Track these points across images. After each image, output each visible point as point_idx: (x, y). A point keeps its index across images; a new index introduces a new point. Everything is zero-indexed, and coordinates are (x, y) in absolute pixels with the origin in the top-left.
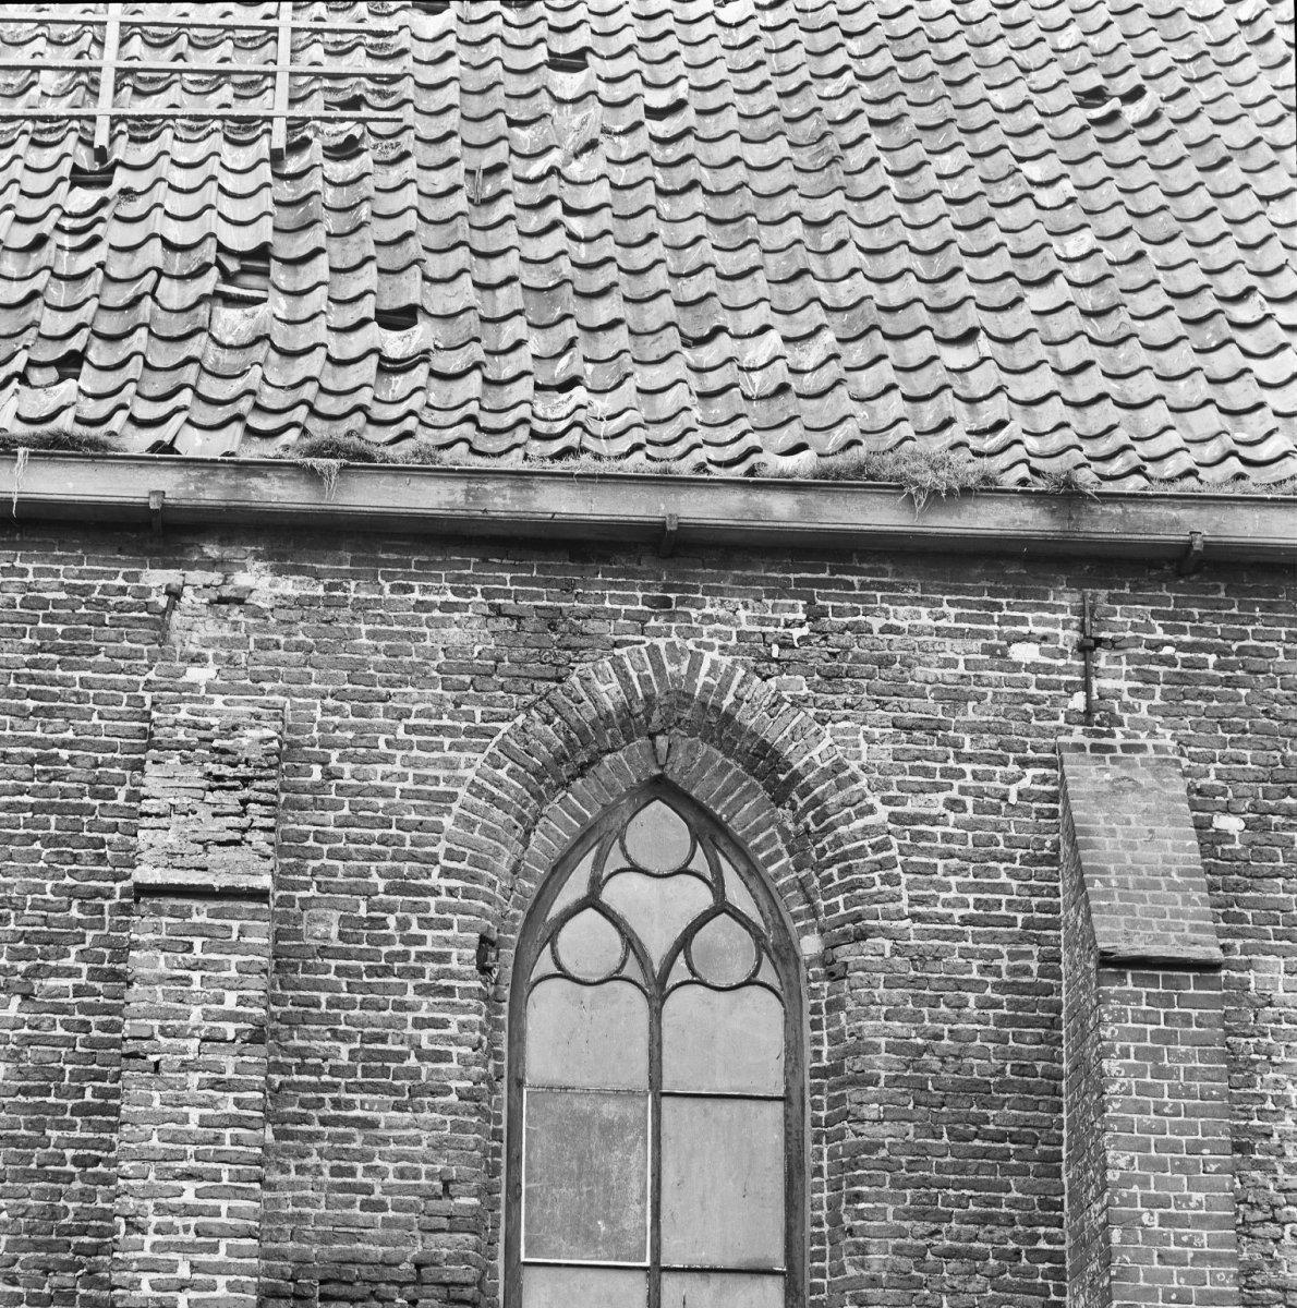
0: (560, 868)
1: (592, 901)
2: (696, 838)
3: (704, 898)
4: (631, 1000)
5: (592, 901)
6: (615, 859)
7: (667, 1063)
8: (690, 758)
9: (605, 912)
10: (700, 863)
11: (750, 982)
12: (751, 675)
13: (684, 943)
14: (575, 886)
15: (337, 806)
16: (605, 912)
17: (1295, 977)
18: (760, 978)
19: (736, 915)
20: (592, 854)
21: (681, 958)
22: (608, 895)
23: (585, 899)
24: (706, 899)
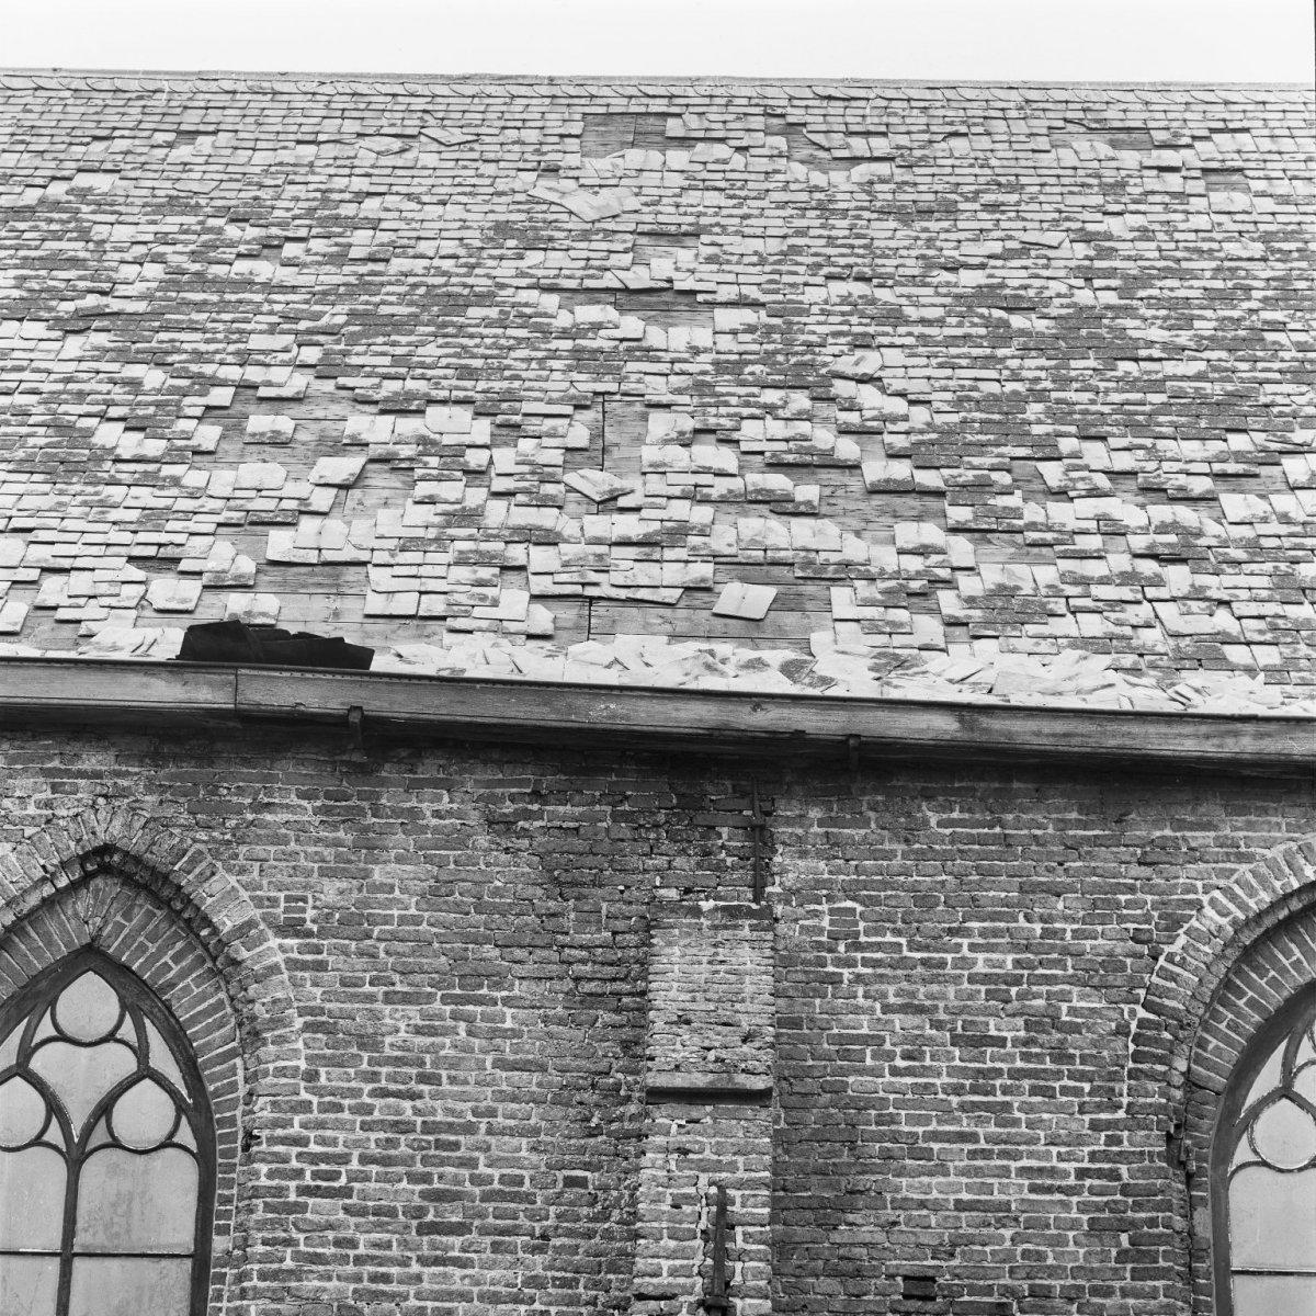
2: (124, 1007)
5: (1286, 1092)
6: (46, 1029)
10: (128, 1031)
13: (105, 1109)
19: (160, 1081)
21: (103, 1122)
22: (36, 1064)
24: (129, 1064)
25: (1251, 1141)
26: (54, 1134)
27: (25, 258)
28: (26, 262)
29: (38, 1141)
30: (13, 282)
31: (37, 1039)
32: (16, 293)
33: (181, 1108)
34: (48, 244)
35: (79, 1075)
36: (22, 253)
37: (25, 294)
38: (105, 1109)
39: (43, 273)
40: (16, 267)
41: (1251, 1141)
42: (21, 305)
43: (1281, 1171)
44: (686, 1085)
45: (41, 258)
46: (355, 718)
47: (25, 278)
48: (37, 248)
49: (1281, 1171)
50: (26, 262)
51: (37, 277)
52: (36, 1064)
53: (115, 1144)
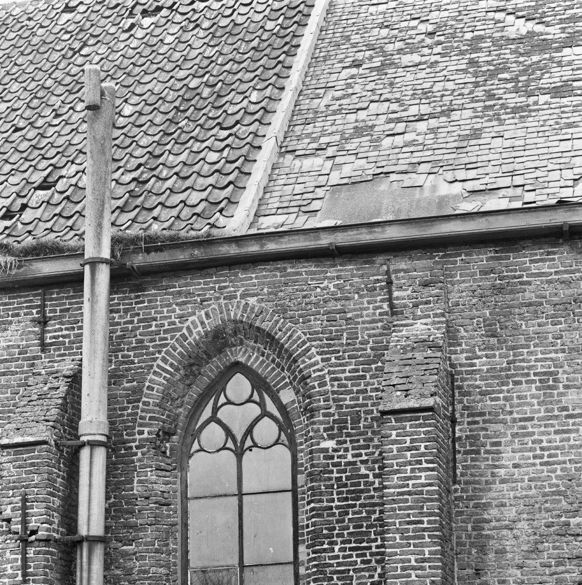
0: (199, 405)
1: (214, 418)
3: (256, 410)
4: (228, 457)
5: (214, 418)
6: (222, 400)
7: (239, 487)
8: (247, 354)
9: (220, 422)
10: (256, 397)
11: (276, 443)
12: (53, 76)
13: (249, 431)
14: (207, 413)
15: (376, 540)
16: (220, 422)
17: (581, 488)
18: (225, 401)
20: (212, 401)
21: (249, 437)
23: (211, 417)
25: (199, 442)
26: (230, 444)
27: (560, 19)
28: (561, 21)
29: (224, 448)
30: (560, 31)
31: (219, 404)
32: (563, 35)
33: (281, 429)
34: (568, 12)
35: (237, 417)
36: (558, 17)
37: (568, 35)
38: (249, 431)
39: (571, 24)
40: (558, 24)
41: (199, 442)
42: (568, 40)
43: (209, 452)
44: (407, 407)
45: (567, 18)
46: (566, 228)
47: (565, 28)
48: (564, 14)
49: (209, 452)
50: (561, 21)
51: (570, 27)
52: (219, 415)
53: (255, 445)
